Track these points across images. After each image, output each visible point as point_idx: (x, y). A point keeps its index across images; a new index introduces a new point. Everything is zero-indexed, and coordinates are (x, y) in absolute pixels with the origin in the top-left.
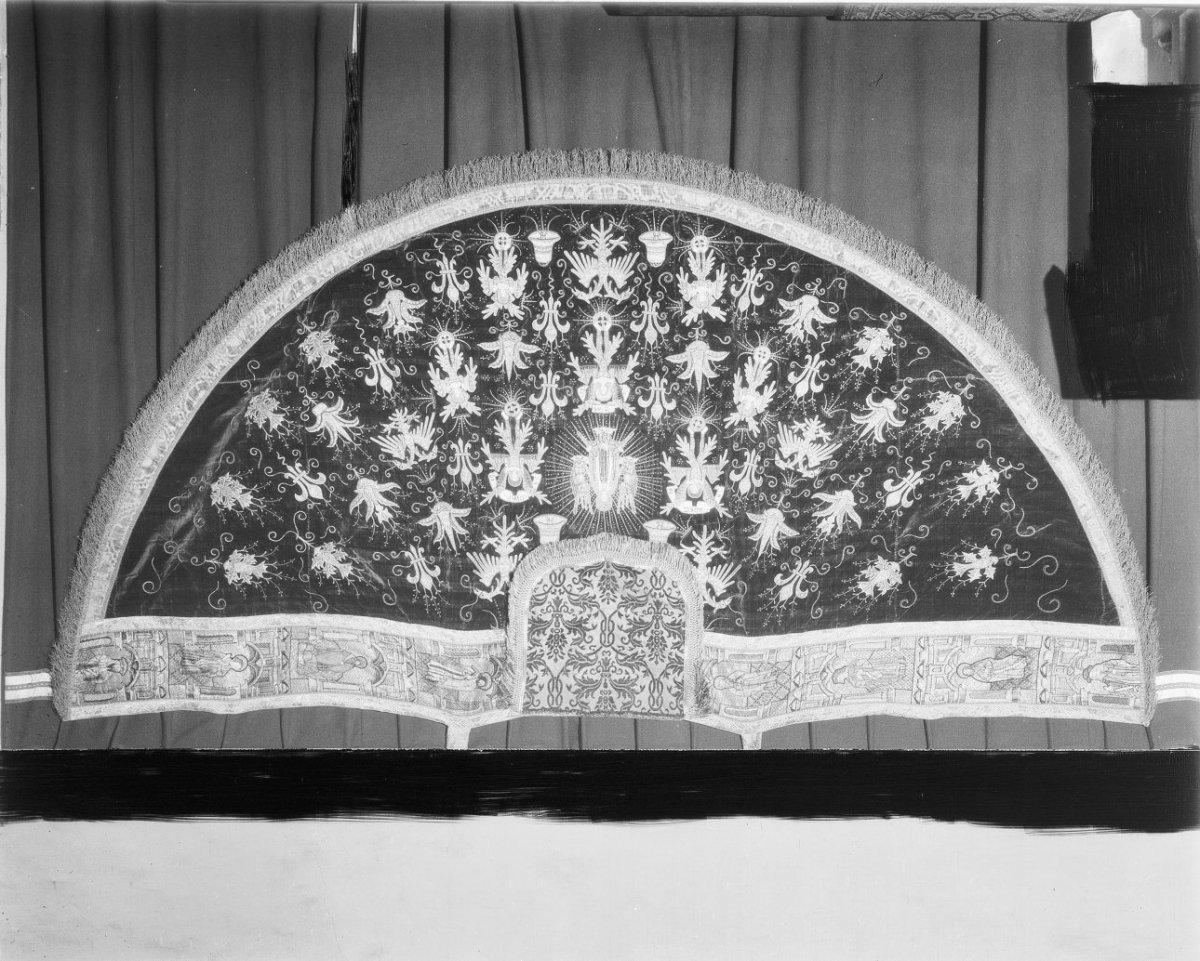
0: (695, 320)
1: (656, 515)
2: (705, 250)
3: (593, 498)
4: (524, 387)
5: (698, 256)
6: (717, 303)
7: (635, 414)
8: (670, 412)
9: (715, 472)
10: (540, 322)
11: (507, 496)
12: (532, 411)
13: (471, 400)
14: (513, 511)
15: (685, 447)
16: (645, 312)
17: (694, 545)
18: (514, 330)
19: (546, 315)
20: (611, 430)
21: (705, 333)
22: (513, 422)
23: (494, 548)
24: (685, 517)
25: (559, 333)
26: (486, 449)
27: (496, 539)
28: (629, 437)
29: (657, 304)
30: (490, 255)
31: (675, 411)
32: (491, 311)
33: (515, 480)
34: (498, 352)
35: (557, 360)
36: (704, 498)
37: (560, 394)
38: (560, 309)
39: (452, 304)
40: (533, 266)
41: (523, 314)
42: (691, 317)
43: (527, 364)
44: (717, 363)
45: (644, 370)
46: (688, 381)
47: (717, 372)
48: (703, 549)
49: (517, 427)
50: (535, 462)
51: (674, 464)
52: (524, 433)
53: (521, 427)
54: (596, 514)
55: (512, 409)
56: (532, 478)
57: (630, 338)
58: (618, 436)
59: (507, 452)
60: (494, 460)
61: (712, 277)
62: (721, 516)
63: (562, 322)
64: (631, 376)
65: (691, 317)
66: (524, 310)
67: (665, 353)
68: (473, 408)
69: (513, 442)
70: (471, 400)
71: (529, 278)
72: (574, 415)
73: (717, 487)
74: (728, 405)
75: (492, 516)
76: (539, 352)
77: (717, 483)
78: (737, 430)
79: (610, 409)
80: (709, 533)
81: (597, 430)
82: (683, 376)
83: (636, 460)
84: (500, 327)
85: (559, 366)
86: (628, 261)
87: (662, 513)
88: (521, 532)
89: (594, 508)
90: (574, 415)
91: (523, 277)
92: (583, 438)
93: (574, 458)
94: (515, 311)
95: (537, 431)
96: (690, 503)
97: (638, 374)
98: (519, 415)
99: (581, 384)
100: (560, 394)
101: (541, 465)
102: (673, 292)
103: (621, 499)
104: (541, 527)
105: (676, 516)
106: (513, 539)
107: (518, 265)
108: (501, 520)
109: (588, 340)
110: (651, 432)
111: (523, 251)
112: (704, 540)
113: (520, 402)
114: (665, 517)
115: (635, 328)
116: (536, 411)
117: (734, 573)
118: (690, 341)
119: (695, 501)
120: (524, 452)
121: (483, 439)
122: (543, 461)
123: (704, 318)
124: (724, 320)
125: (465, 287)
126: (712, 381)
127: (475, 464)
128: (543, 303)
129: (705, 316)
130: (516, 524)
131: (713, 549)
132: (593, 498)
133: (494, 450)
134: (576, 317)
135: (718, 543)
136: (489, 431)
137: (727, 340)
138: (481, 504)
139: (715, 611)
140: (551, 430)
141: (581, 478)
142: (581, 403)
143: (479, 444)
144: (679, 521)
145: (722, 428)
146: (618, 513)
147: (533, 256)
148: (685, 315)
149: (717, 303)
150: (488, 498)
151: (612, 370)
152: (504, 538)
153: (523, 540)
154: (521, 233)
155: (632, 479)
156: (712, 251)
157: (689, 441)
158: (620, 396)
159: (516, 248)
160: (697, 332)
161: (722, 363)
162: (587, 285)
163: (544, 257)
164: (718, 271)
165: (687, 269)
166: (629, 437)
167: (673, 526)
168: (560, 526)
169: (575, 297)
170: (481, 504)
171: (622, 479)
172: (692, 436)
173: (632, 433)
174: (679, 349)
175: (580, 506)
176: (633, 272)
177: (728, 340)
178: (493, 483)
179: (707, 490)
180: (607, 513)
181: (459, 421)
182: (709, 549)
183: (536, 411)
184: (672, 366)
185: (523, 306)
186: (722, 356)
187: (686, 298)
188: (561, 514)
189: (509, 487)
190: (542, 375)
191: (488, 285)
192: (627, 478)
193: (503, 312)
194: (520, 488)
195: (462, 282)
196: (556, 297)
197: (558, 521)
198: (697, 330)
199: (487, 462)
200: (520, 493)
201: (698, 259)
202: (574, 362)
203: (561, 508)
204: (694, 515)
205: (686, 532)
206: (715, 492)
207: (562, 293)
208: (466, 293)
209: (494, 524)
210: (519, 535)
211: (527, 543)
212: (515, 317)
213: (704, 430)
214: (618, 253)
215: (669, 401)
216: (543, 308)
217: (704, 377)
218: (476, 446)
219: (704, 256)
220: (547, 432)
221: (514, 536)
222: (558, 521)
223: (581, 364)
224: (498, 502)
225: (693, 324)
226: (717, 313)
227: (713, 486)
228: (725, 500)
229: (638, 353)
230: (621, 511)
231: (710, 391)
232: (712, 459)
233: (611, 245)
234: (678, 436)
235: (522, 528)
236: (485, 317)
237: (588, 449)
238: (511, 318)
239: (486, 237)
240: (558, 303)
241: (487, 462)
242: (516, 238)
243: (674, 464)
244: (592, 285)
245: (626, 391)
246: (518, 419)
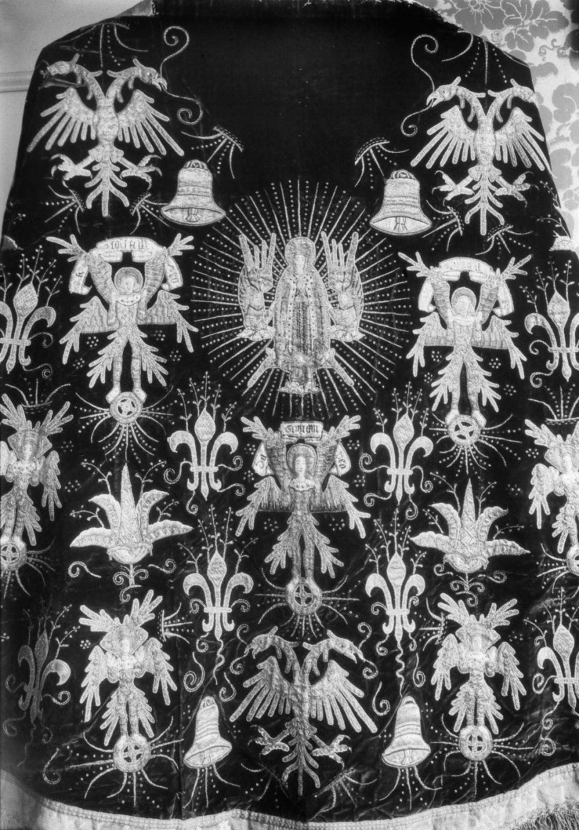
0: (136, 601)
1: (200, 233)
2: (122, 742)
3: (320, 263)
4: (442, 469)
5: (136, 728)
6: (96, 638)
7: (244, 420)
8: (181, 426)
9: (89, 320)
10: (413, 591)
11: (479, 269)
12: (430, 422)
13: (543, 449)
14: (469, 244)
15: (148, 361)
16: (227, 610)
17: (125, 179)
18: (459, 575)
19: (404, 605)
20: (293, 387)
21: (117, 578)
22: (465, 407)
23: (504, 176)
24: (143, 232)
25: (383, 573)
26: (517, 358)
27: (499, 192)
28: (257, 375)
29: (207, 628)
30: (501, 717)
31: (171, 430)
32: (502, 614)
33: (465, 297)
34: (490, 538)
35: (387, 519)
36: (109, 268)
37: (382, 456)
38: (384, 618)
39: (566, 623)
40: (424, 696)
41: (440, 605)
42: (143, 610)
43: (435, 512)
44: (95, 523)
45: (229, 501)
46: (148, 487)
47: (93, 507)
48: (107, 173)
49: (457, 396)
50: (429, 333)
51: (171, 329)
52: (445, 385)
53: (450, 395)
54: (315, 232)
55: (465, 431)
56: (433, 302)
57: (254, 565)
58: (277, 377)
59: (478, 350)
60: (502, 336)
61: (107, 689)
62: (73, 238)
63: (378, 594)
64: (250, 489)
65: (143, 610)
66: (438, 611)
67: (194, 539)
68: (539, 434)
69: (464, 368)
70: (543, 449)
71: (429, 671)
72: (358, 418)
73: (85, 291)
74: (69, 445)
75: (506, 235)
76: (414, 533)
77: (86, 298)
78: (47, 402)
79: (290, 429)
80: (98, 201)
81: (311, 387)
82: (157, 495)
83: (243, 335)
84: (484, 581)
85: (384, 509)
86: (256, 705)
87: (190, 238)
88: (452, 203)
89: (320, 244)
90: (358, 418)
91: (441, 675)
92: (341, 372)
93: (358, 336)
94: (455, 610)
95: (423, 385)
96: (137, 258)
97: (238, 493)
98: (453, 416)
99: (344, 478)
100: (382, 456)
101: (420, 325)
102: (178, 652)
103: (269, 263)
104: (417, 211)
105: (163, 233)
106: (469, 192)
107: (449, 696)
108: (489, 228)
109: (329, 560)
110: (214, 387)
111: (439, 727)
112: (106, 187)
113: (449, 442)
114: (186, 230)
115: (243, 579)
116: (424, 426)
117: (43, 132)
118: (143, 563)
119: (127, 260)
120: (447, 350)
121: (522, 376)
122: (415, 332)
123: (119, 606)
124: (84, 609)
125: (544, 654)
126: (102, 489)
127: (540, 332)
128: (411, 628)
129: (120, 611)
130: (462, 218)
131: (88, 173)
132: (320, 263)
133: (504, 355)
134: (352, 606)
135: (79, 184)
136: (512, 390)
137: (75, 569)
138: (528, 258)
139: (77, 57)
140: (402, 390)
141: (344, 299)
142: (345, 441)
143: (529, 367)
144: (156, 222)
145: (75, 402)
146: (274, 236)
147: (423, 715)
148: (156, 611)
149: (96, 638)
150: (514, 269)
151: (287, 502)
152: (484, 194)
153: (451, 188)
154: (441, 757)
155: (251, 298)
156: (107, 742)
157: (144, 375)
158: (271, 453)
159: (451, 728)
160: (132, 581)
161: (83, 525)
162: (334, 665)
163: (409, 712)
164: (98, 704)
165: (155, 700)
166: (257, 375)
167: (169, 215)
168: (385, 210)
169: (356, 644)
170: (528, 258)
171: (269, 296)
172: (137, 384)
173: (251, 383)
174: (164, 548)
175: (346, 249)
176: (247, 684)
177: (74, 571)
178: (505, 296)
179: (103, 279)
180: (295, 232)
181: (567, 411)
182: (95, 174)
183: (424, 426)
184: (178, 514)
185: (442, 619)
186: (84, 539)
187: (156, 645)
188: (383, 235)
189: (476, 287)
190: (411, 490)
191: (506, 660)
192: (258, 300)
193: (480, 609)
194: (454, 285)
195: (548, 663)
196: (391, 642)
197: (384, 222)
198: (132, 584)
199: (516, 335)
200: (455, 277)
201: (134, 720)
202: (356, 519)
203: (381, 247)
204: (127, 235)
205: (143, 204)
206: (89, 281)
207: (380, 650)
208: (542, 645)
209: (502, 220)
210: (455, 198)
211: (443, 183)
212: (456, 598)
213: (114, 395)
214: (277, 723)
215: (184, 449)
216: (410, 617)
217: (117, 495)
218: (535, 363)
219: (125, 728)
220: (409, 386)
221: (467, 197)
222: (384, 222)
223: (345, 516)
224: (497, 261)
225: (141, 595)
226: (96, 620)
227: (94, 292)
228: (66, 267)
229: (238, 533)
230: (267, 238)
231: (105, 470)
232: (94, 344)
233: (286, 741)
234: (163, 382)
235: (452, 211)
236: (514, 601)
237: (333, 352)
238: (464, 597)
239: (506, 751)
240: (387, 630)
241: (516, 335)
242: (449, 747)
243: (171, 329)
244: (322, 666)
245: (260, 466)
246: (455, 411)
